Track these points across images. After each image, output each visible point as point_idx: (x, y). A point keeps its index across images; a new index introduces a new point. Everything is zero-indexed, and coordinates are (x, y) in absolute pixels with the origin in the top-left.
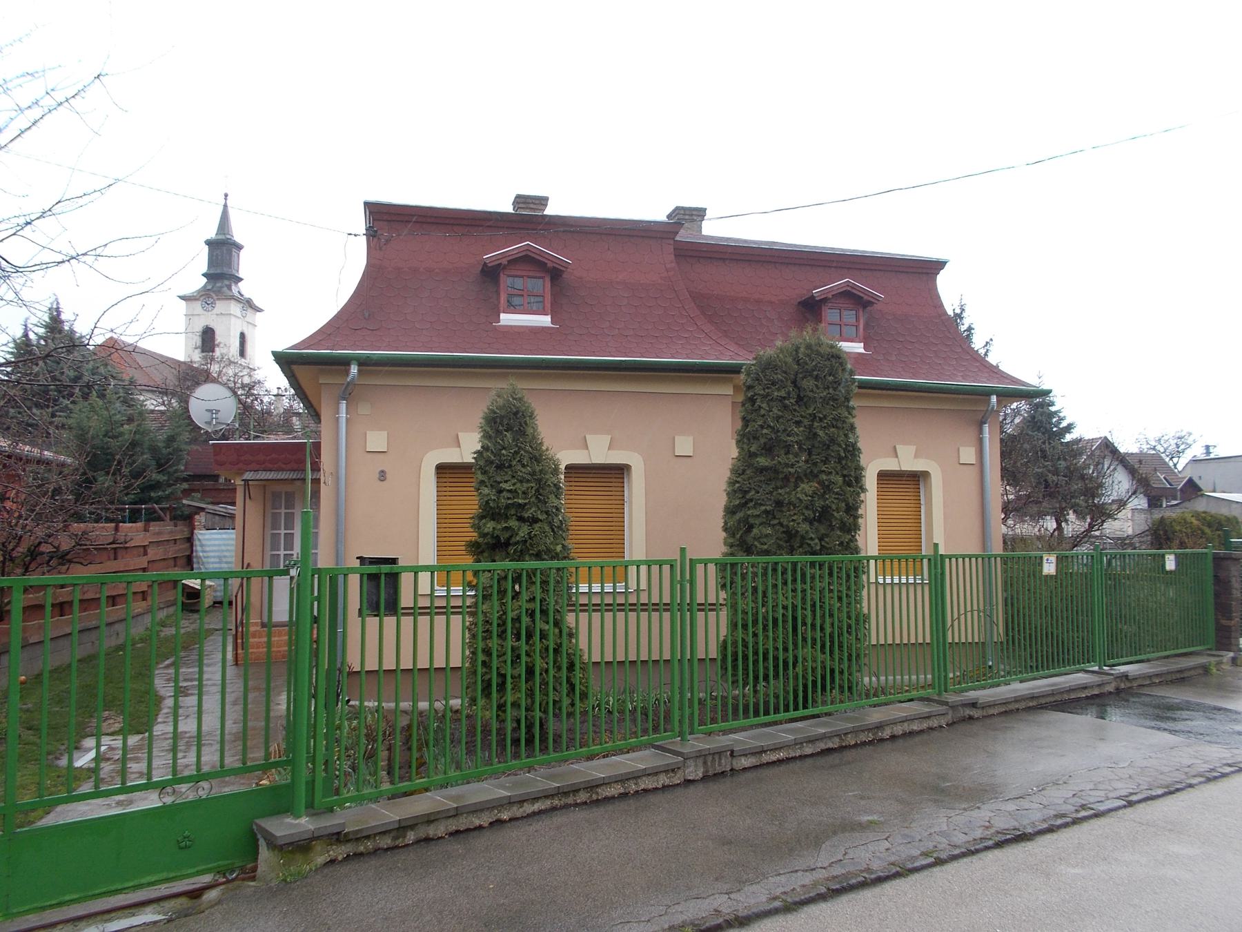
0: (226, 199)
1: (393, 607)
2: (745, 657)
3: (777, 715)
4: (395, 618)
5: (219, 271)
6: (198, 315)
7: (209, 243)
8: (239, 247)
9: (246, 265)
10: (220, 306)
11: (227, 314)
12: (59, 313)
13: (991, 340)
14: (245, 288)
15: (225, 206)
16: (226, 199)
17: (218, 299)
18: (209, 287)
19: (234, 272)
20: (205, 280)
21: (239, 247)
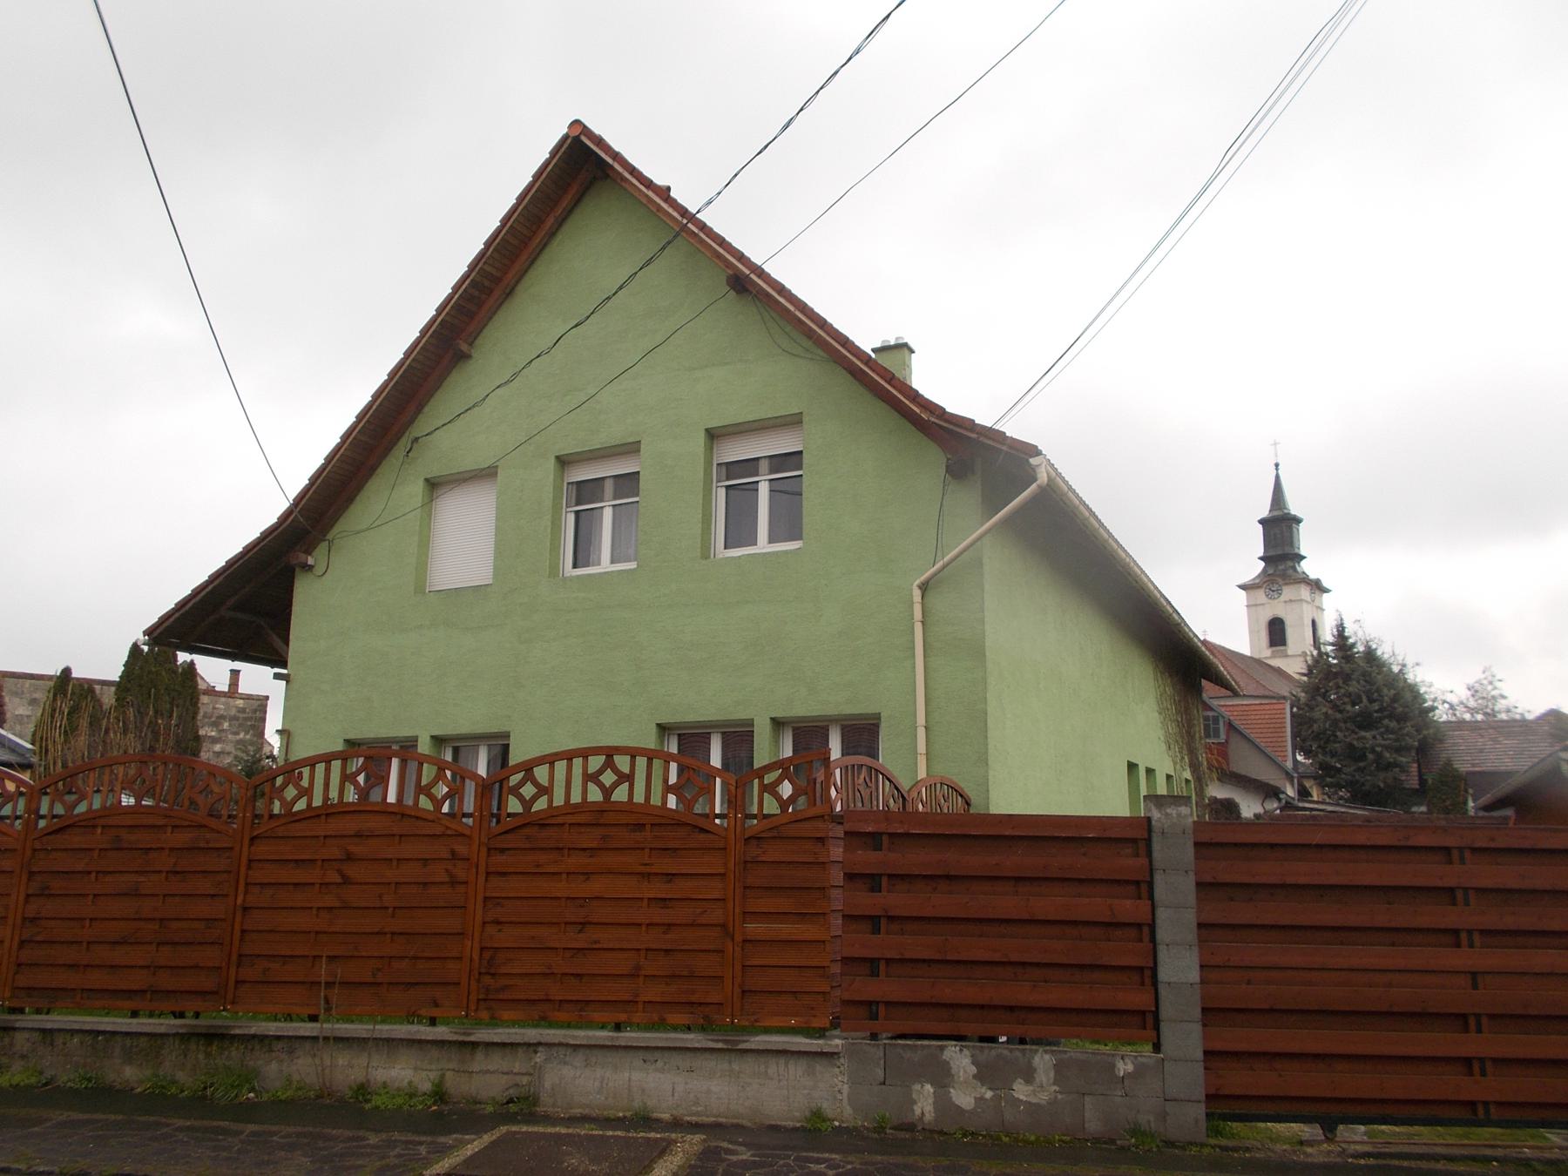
0: (1277, 469)
2: (51, 729)
5: (1280, 552)
6: (1263, 604)
7: (1262, 522)
8: (1298, 521)
9: (1307, 541)
10: (1288, 592)
11: (1298, 600)
12: (1343, 628)
14: (1309, 567)
15: (1277, 478)
16: (1277, 469)
17: (1286, 584)
18: (1271, 571)
19: (1296, 551)
20: (1262, 564)
21: (1298, 521)
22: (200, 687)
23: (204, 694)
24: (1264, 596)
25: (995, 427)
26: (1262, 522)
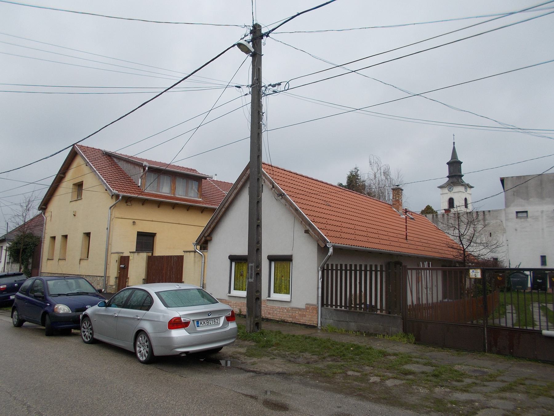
0: (454, 145)
1: (5, 239)
3: (366, 264)
4: (135, 251)
6: (447, 193)
7: (448, 163)
9: (464, 169)
10: (457, 189)
13: (356, 165)
14: (465, 179)
16: (454, 145)
20: (448, 179)
22: (32, 260)
23: (373, 308)
24: (448, 191)
25: (9, 231)
26: (448, 163)
